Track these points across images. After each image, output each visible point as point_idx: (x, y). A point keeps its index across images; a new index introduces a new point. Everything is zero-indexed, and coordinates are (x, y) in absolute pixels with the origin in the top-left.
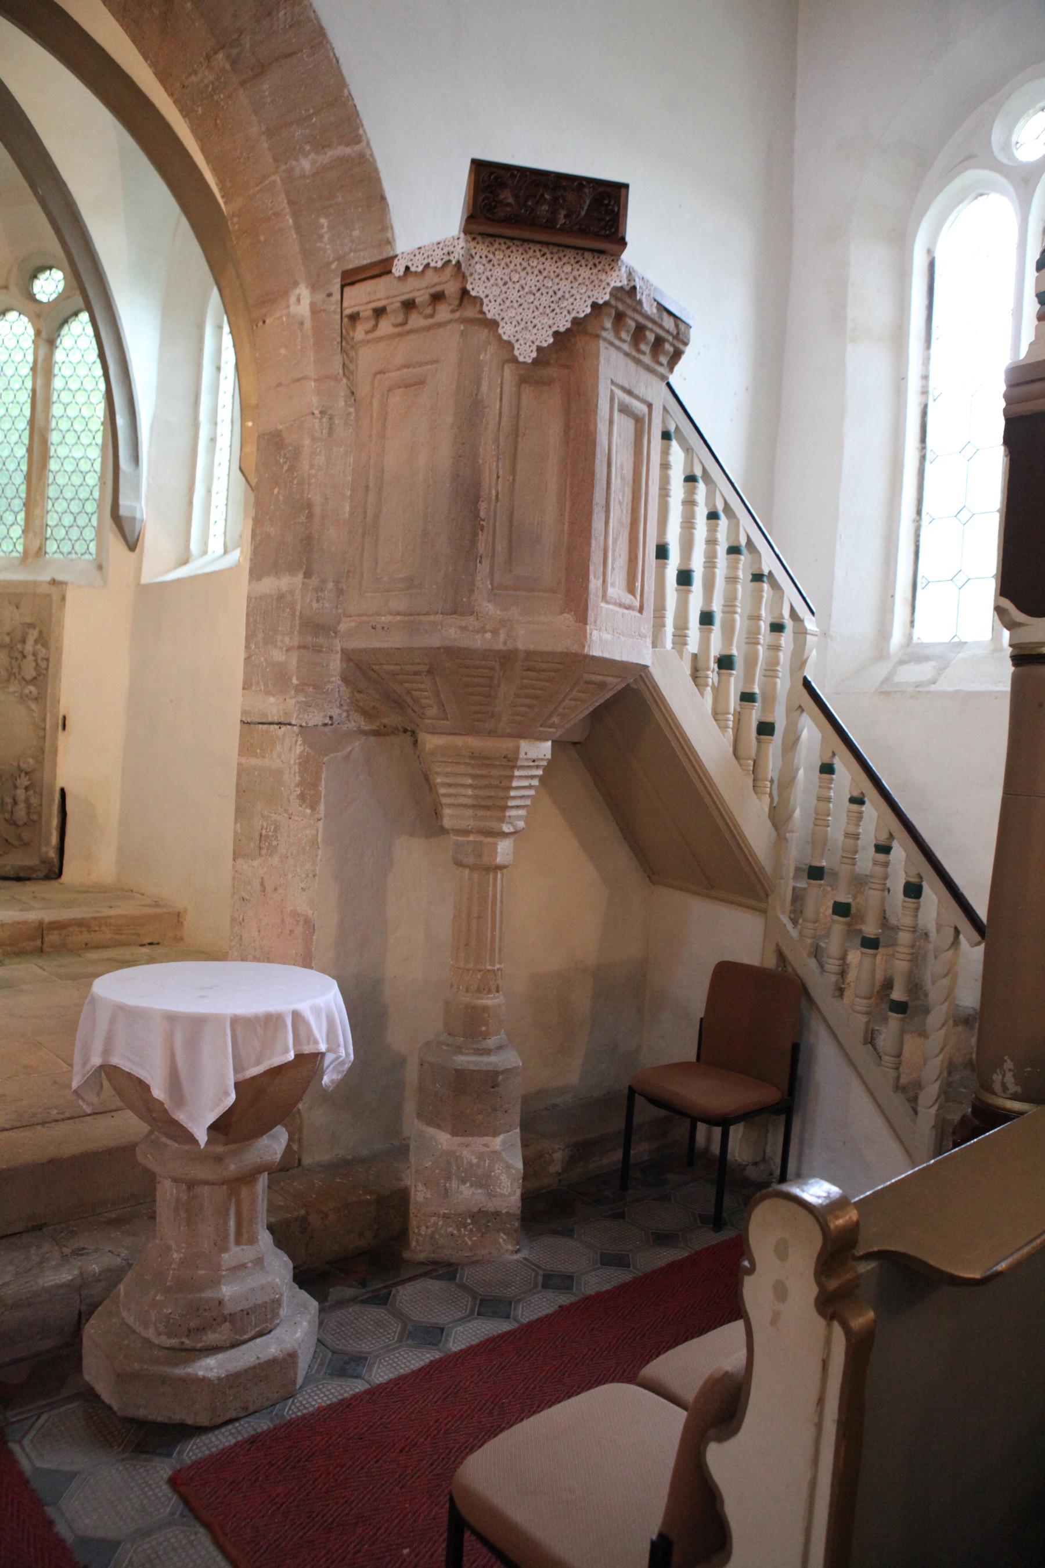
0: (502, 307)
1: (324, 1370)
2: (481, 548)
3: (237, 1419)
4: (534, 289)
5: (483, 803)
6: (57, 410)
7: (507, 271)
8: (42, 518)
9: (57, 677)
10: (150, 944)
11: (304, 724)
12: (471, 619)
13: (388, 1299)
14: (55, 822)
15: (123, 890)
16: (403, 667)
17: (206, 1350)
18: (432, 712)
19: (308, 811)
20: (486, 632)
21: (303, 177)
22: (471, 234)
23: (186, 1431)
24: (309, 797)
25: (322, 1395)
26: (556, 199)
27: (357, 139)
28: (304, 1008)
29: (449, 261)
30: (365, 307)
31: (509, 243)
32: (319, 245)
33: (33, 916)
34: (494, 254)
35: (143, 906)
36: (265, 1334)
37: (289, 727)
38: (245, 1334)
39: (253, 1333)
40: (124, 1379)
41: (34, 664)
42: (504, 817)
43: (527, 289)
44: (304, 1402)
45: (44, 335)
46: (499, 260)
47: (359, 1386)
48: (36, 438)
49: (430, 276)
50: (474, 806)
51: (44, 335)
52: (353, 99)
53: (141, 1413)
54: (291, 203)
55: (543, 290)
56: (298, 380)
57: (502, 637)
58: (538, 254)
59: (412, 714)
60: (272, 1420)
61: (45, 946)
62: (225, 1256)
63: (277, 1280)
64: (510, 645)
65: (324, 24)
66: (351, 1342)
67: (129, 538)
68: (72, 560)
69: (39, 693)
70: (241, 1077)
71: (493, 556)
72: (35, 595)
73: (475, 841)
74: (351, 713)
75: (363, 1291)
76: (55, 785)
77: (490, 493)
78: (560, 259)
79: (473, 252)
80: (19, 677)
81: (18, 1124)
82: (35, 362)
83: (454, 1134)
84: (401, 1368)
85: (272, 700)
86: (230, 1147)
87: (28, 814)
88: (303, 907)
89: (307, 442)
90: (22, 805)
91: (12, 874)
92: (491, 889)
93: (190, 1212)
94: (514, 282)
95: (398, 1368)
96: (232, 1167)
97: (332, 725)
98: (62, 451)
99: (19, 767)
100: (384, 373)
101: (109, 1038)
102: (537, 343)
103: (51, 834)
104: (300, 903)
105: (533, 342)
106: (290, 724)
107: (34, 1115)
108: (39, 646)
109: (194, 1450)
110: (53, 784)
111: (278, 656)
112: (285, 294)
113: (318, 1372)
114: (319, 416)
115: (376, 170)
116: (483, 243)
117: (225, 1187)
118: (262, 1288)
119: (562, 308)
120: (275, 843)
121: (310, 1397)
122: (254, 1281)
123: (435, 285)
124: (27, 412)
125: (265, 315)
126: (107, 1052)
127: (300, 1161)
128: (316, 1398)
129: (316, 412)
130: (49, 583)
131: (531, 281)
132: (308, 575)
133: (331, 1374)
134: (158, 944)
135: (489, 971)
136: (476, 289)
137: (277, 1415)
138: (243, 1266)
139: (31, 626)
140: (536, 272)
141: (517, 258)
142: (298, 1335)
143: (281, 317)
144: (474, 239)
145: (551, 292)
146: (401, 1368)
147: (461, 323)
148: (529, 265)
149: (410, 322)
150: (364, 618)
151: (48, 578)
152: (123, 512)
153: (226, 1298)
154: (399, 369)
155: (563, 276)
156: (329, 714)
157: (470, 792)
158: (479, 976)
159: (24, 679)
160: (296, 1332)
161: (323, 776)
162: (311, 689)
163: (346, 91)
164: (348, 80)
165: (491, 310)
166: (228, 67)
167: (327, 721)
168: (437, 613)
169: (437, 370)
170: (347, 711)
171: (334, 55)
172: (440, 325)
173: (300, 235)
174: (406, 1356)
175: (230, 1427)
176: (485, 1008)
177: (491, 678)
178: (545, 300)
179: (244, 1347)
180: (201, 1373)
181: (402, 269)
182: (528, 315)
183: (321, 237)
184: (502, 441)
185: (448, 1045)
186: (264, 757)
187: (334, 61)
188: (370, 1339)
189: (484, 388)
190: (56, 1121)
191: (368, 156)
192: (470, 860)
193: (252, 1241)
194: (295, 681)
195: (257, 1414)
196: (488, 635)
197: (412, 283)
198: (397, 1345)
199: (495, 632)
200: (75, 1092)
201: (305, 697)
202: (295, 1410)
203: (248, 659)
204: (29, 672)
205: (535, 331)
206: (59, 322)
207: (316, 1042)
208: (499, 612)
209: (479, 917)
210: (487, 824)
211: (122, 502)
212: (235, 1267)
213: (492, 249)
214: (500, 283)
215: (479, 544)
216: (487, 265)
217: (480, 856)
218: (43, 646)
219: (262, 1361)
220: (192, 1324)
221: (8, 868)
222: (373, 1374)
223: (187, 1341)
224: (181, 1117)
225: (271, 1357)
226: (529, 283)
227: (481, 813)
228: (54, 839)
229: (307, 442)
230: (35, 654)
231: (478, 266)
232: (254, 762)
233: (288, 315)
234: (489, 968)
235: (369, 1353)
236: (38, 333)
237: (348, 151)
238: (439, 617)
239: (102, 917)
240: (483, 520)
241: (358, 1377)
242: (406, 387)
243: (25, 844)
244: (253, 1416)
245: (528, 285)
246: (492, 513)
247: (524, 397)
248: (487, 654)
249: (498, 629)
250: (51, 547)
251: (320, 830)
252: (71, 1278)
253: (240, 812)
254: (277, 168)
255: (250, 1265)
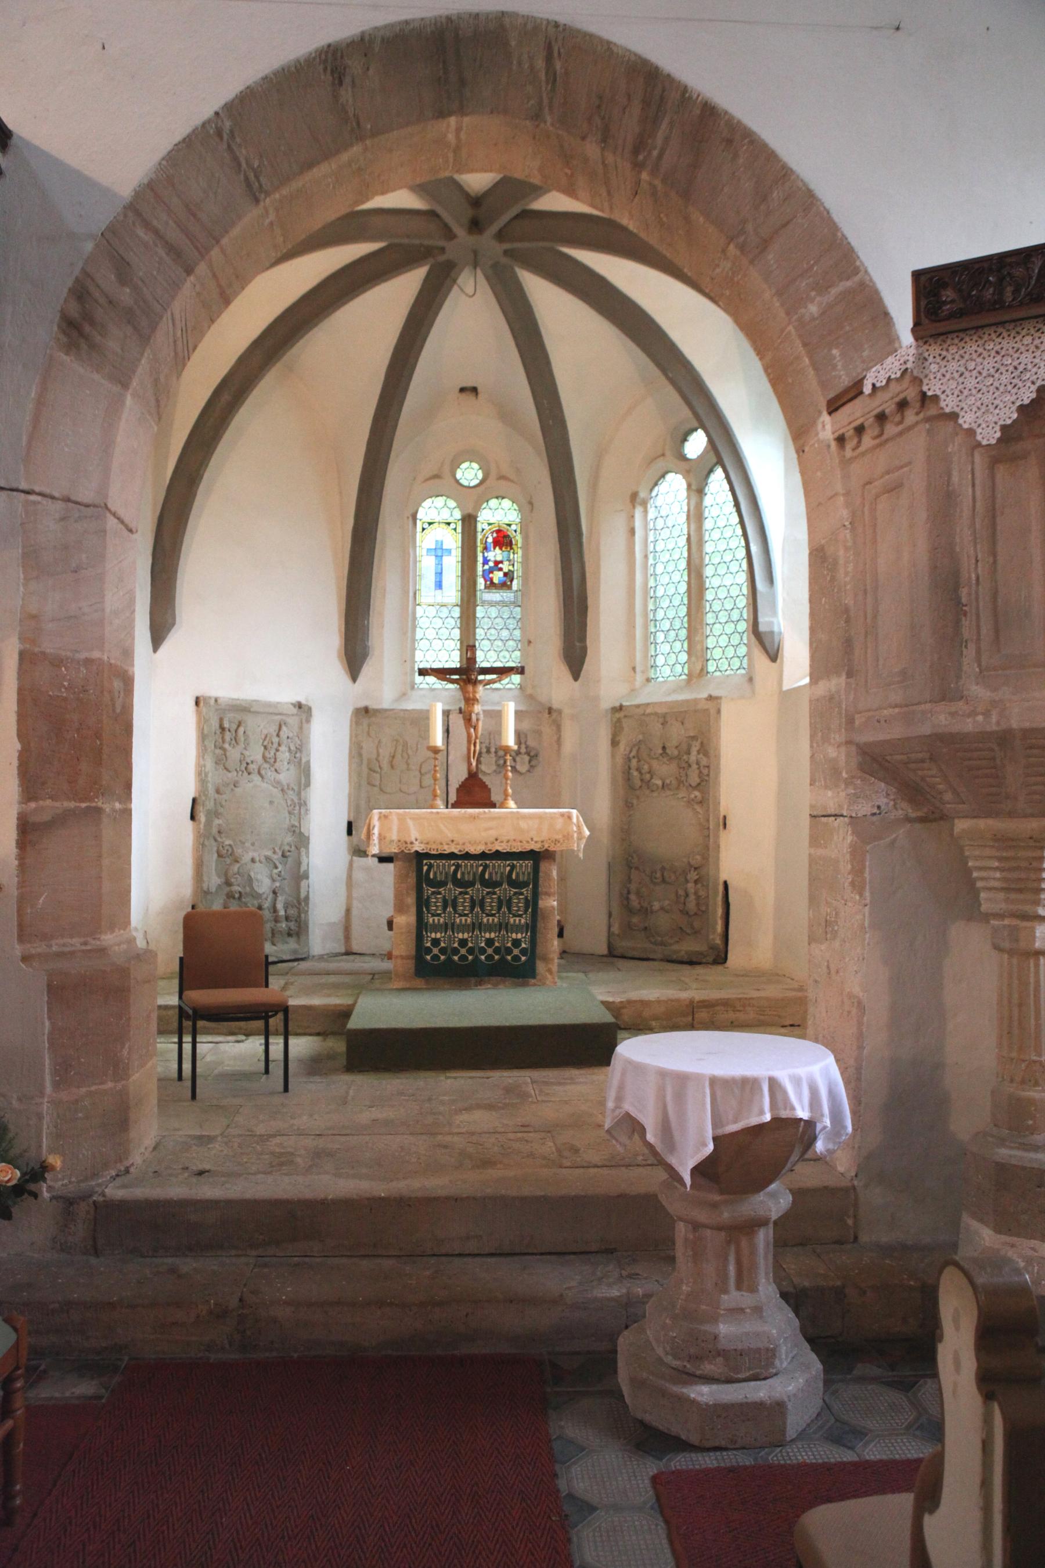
0: (960, 398)
1: (821, 1433)
2: (966, 633)
3: (726, 1449)
4: (992, 371)
5: (1013, 886)
6: (708, 548)
7: (962, 362)
8: (702, 642)
9: (717, 783)
10: (792, 1025)
11: (854, 815)
12: (961, 703)
13: (912, 1387)
14: (720, 911)
15: (778, 975)
16: (909, 755)
17: (708, 1379)
18: (948, 796)
19: (857, 897)
20: (977, 714)
21: (813, 319)
22: (922, 338)
23: (683, 1446)
24: (858, 887)
25: (810, 1453)
26: (1001, 280)
27: (856, 271)
28: (783, 1076)
29: (907, 369)
30: (848, 428)
31: (961, 335)
32: (834, 373)
33: (685, 995)
34: (947, 350)
35: (787, 989)
36: (760, 1380)
37: (842, 818)
38: (738, 1373)
39: (748, 1374)
40: (638, 1384)
41: (697, 772)
42: (1040, 899)
43: (985, 373)
44: (791, 1454)
45: (694, 487)
46: (953, 354)
47: (849, 1456)
48: (693, 576)
49: (894, 388)
50: (1002, 889)
51: (694, 487)
52: (846, 239)
53: (647, 1418)
54: (805, 345)
55: (1003, 369)
56: (831, 497)
57: (994, 719)
58: (994, 336)
59: (933, 800)
60: (755, 1459)
61: (695, 1022)
62: (725, 1297)
63: (775, 1331)
64: (1004, 726)
65: (812, 186)
66: (859, 1416)
67: (770, 650)
68: (728, 676)
69: (703, 797)
70: (720, 1132)
71: (978, 640)
72: (696, 711)
73: (1009, 926)
74: (899, 802)
75: (890, 1374)
76: (719, 878)
77: (970, 578)
78: (1018, 333)
79: (926, 355)
80: (687, 784)
81: (608, 1164)
82: (689, 511)
83: (998, 1230)
84: (898, 1453)
85: (830, 793)
86: (726, 1197)
87: (698, 905)
88: (857, 990)
89: (841, 553)
90: (692, 897)
91: (685, 959)
92: (1032, 975)
93: (697, 1255)
94: (970, 371)
95: (895, 1452)
96: (726, 1215)
97: (880, 814)
98: (715, 582)
99: (689, 863)
100: (871, 483)
101: (621, 1087)
102: (1002, 422)
103: (716, 923)
104: (854, 986)
105: (996, 423)
106: (842, 816)
107: (624, 1159)
108: (701, 756)
109: (681, 1462)
110: (717, 878)
111: (832, 752)
112: (814, 423)
113: (815, 1433)
114: (849, 526)
115: (877, 292)
116: (936, 343)
117: (723, 1234)
118: (757, 1335)
119: (1025, 381)
120: (836, 928)
121: (799, 1451)
122: (750, 1326)
123: (898, 394)
124: (686, 554)
125: (803, 446)
126: (619, 1099)
127: (856, 1238)
128: (803, 1454)
129: (847, 523)
130: (707, 699)
131: (989, 364)
132: (849, 675)
133: (827, 1438)
134: (799, 1026)
135: (1035, 1062)
136: (932, 388)
137: (762, 1457)
138: (742, 1310)
139: (694, 738)
140: (993, 353)
141: (971, 347)
142: (790, 1388)
143: (814, 444)
144: (926, 343)
145: (1011, 368)
146: (898, 1453)
147: (926, 422)
148: (985, 349)
149: (886, 432)
150: (870, 714)
151: (705, 695)
152: (762, 628)
153: (721, 1335)
154: (882, 477)
155: (1023, 349)
156: (877, 803)
157: (998, 875)
158: (1023, 1066)
159: (690, 785)
160: (790, 1385)
161: (867, 863)
162: (859, 782)
163: (839, 234)
164: (840, 225)
165: (948, 404)
166: (738, 253)
167: (875, 810)
168: (926, 702)
169: (910, 471)
170: (894, 800)
171: (824, 207)
172: (909, 429)
173: (816, 369)
174: (907, 1444)
175: (718, 1453)
176: (1031, 1101)
177: (994, 759)
178: (1005, 378)
179: (735, 1385)
180: (693, 1396)
181: (870, 387)
182: (988, 398)
183: (834, 367)
184: (978, 526)
185: (993, 1136)
186: (826, 847)
187: (825, 213)
188: (878, 1419)
189: (955, 479)
190: (638, 1165)
191: (868, 282)
192: (1007, 945)
193: (753, 1289)
194: (844, 775)
195: (745, 1451)
196: (980, 718)
197: (881, 397)
198: (902, 1432)
199: (987, 714)
200: (608, 1131)
201: (855, 789)
202: (780, 1458)
203: (812, 757)
204: (694, 779)
205: (997, 411)
206: (705, 472)
207: (793, 1108)
208: (989, 694)
209: (1020, 1005)
210: (1020, 907)
211: (761, 619)
212: (734, 1309)
213: (945, 346)
214: (956, 375)
215: (963, 630)
216: (941, 363)
217: (1017, 940)
218: (704, 755)
219: (749, 1401)
220: (692, 1351)
221: (683, 953)
222: (867, 1451)
223: (688, 1366)
224: (673, 1161)
225: (758, 1400)
226: (987, 367)
227: (1013, 896)
228: (719, 928)
229: (841, 553)
230: (698, 763)
231: (933, 366)
232: (820, 852)
233: (818, 440)
234: (1035, 1058)
235: (871, 1431)
236: (689, 486)
237: (848, 284)
238: (928, 706)
239: (746, 999)
240: (966, 605)
241: (852, 1448)
242: (889, 492)
243: (696, 933)
244: (740, 1451)
245: (986, 369)
246: (973, 596)
247: (999, 476)
248: (984, 736)
249: (989, 711)
250: (711, 667)
251: (867, 914)
252: (618, 1294)
253: (813, 899)
254: (790, 320)
255: (748, 1310)
